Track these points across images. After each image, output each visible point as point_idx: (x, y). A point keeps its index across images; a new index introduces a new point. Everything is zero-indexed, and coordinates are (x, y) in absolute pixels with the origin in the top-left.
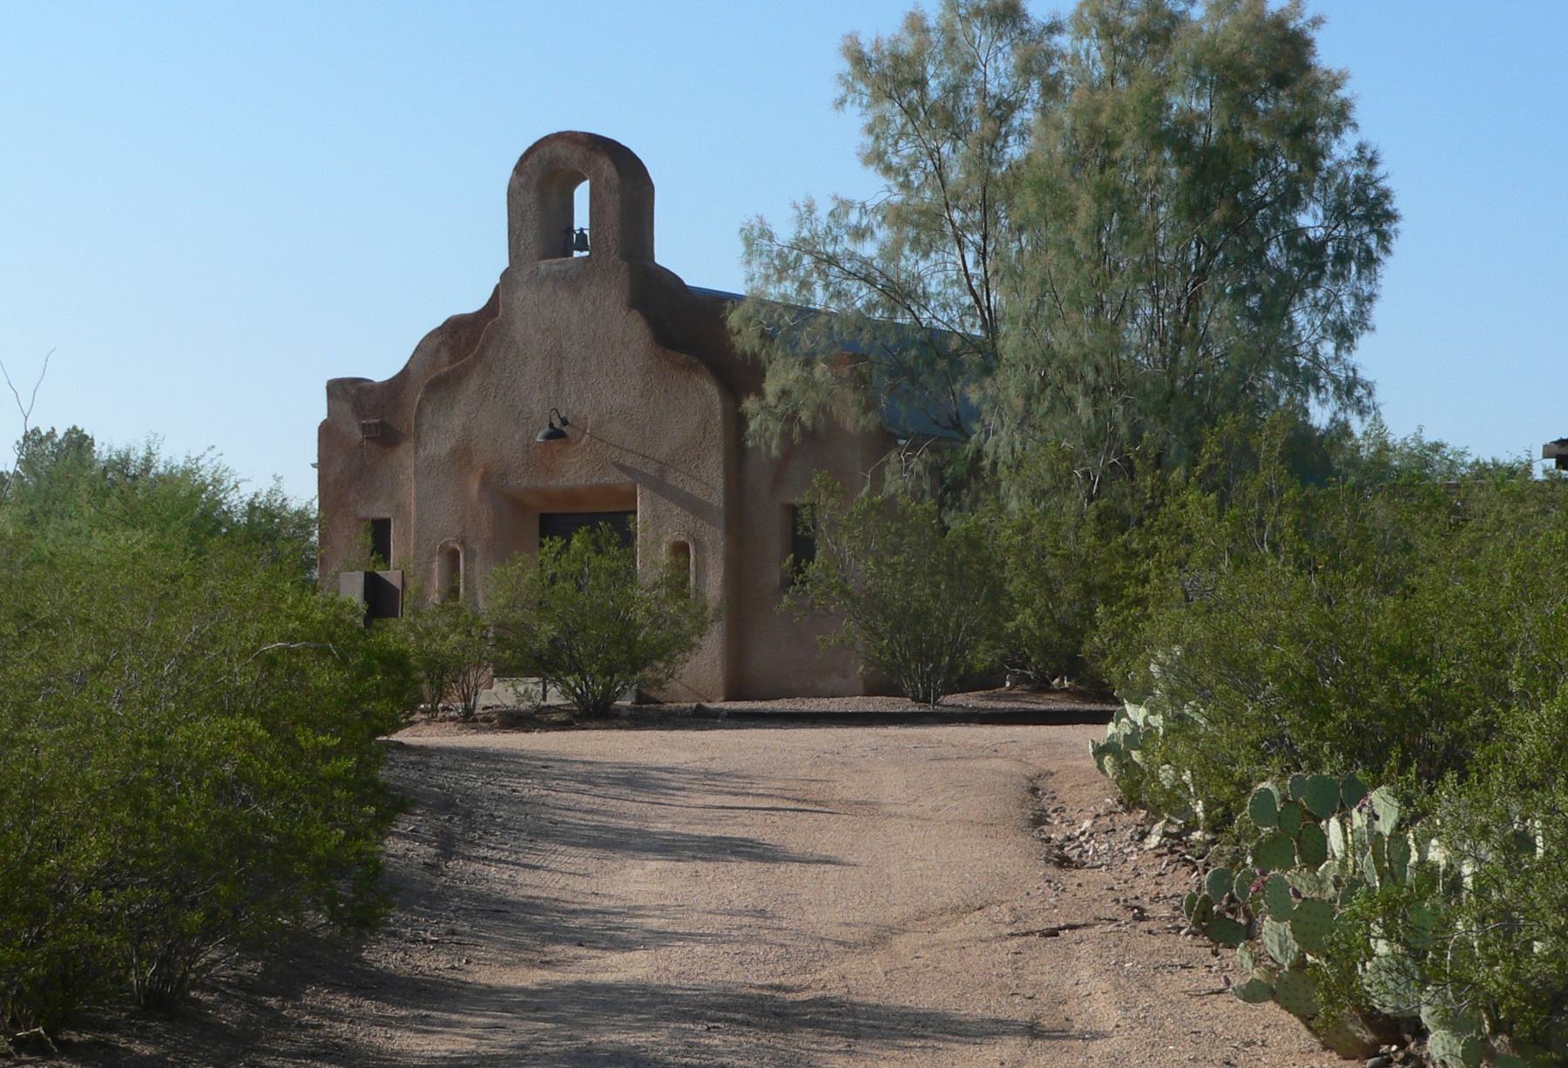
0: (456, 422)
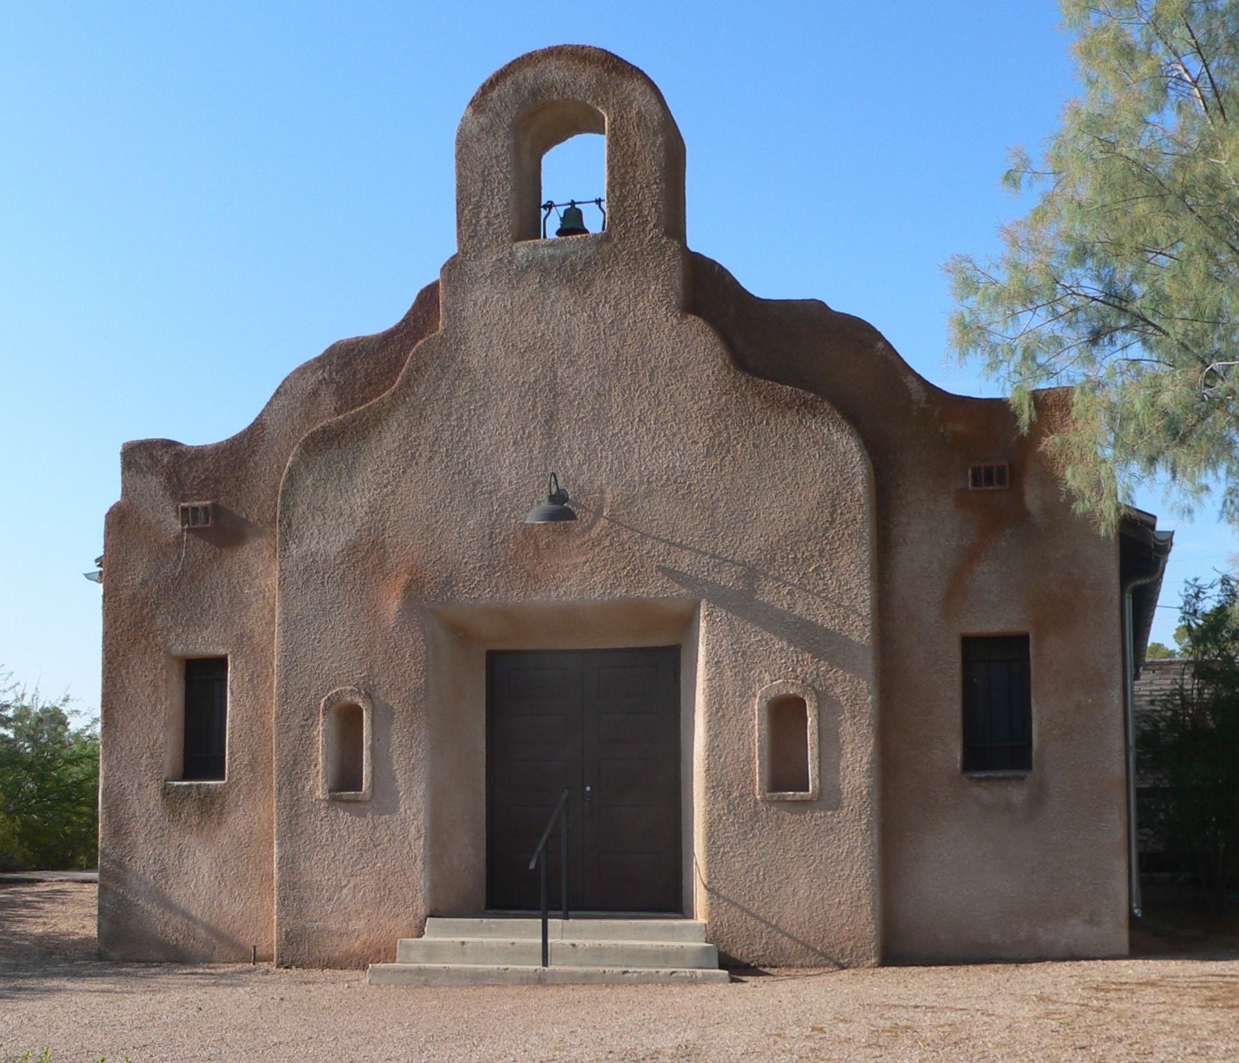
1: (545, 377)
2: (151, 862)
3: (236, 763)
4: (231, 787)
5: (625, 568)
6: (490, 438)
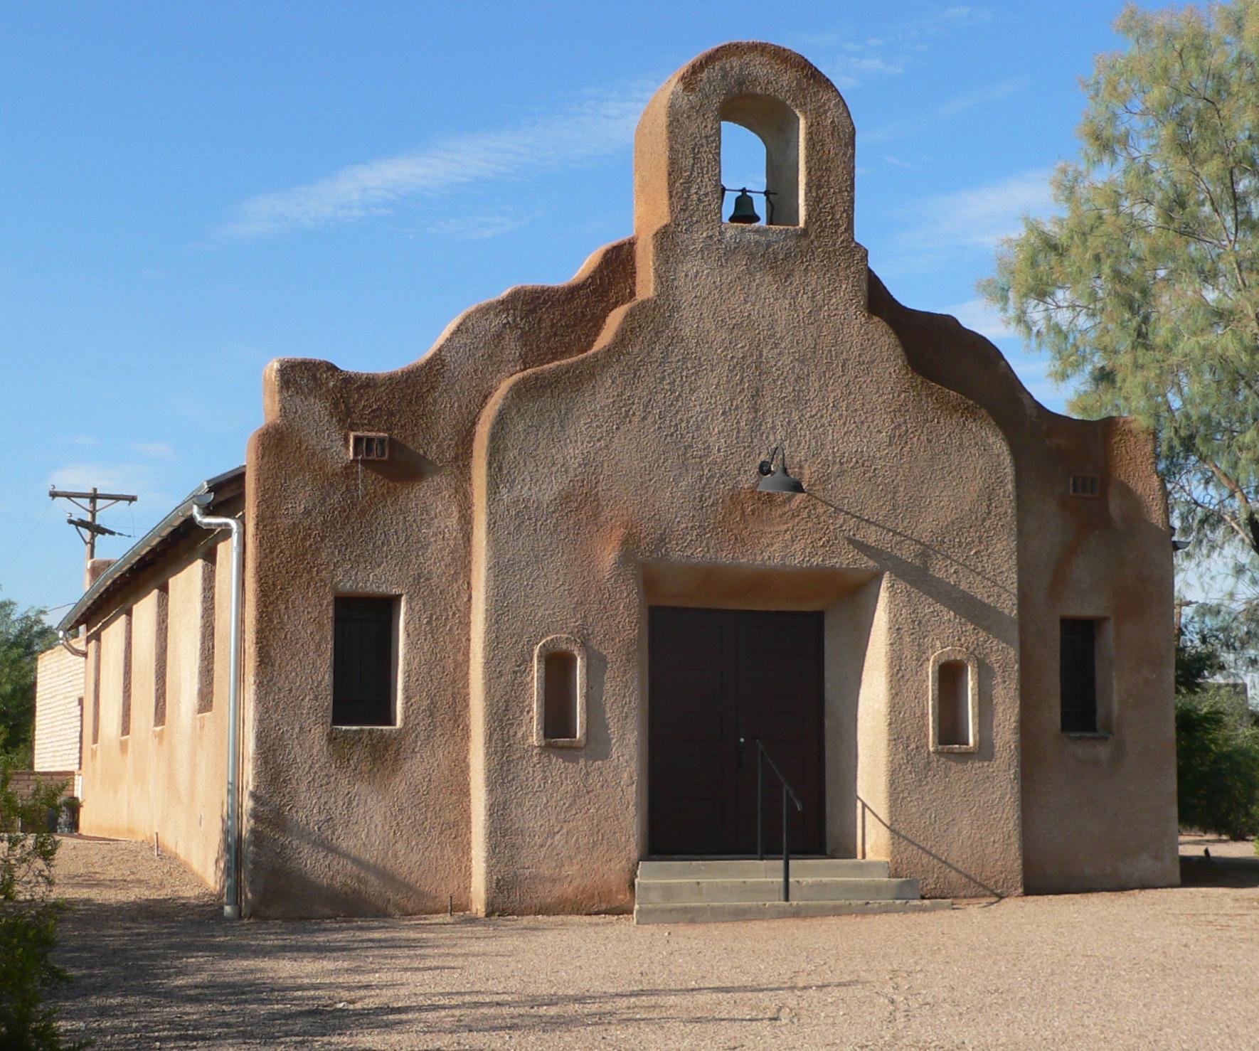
0: (573, 451)
1: (752, 355)
2: (315, 811)
3: (412, 708)
4: (407, 732)
5: (821, 539)
6: (700, 405)
